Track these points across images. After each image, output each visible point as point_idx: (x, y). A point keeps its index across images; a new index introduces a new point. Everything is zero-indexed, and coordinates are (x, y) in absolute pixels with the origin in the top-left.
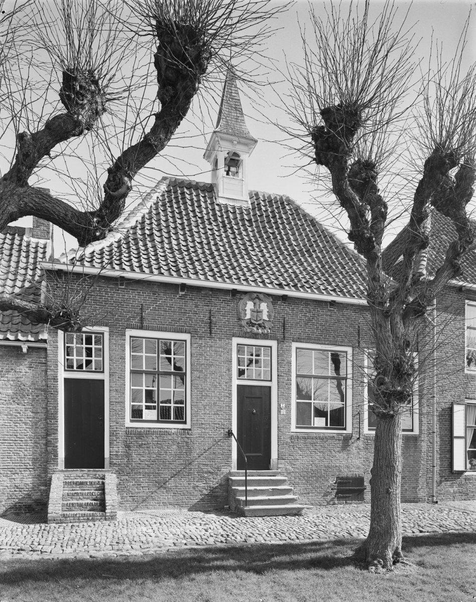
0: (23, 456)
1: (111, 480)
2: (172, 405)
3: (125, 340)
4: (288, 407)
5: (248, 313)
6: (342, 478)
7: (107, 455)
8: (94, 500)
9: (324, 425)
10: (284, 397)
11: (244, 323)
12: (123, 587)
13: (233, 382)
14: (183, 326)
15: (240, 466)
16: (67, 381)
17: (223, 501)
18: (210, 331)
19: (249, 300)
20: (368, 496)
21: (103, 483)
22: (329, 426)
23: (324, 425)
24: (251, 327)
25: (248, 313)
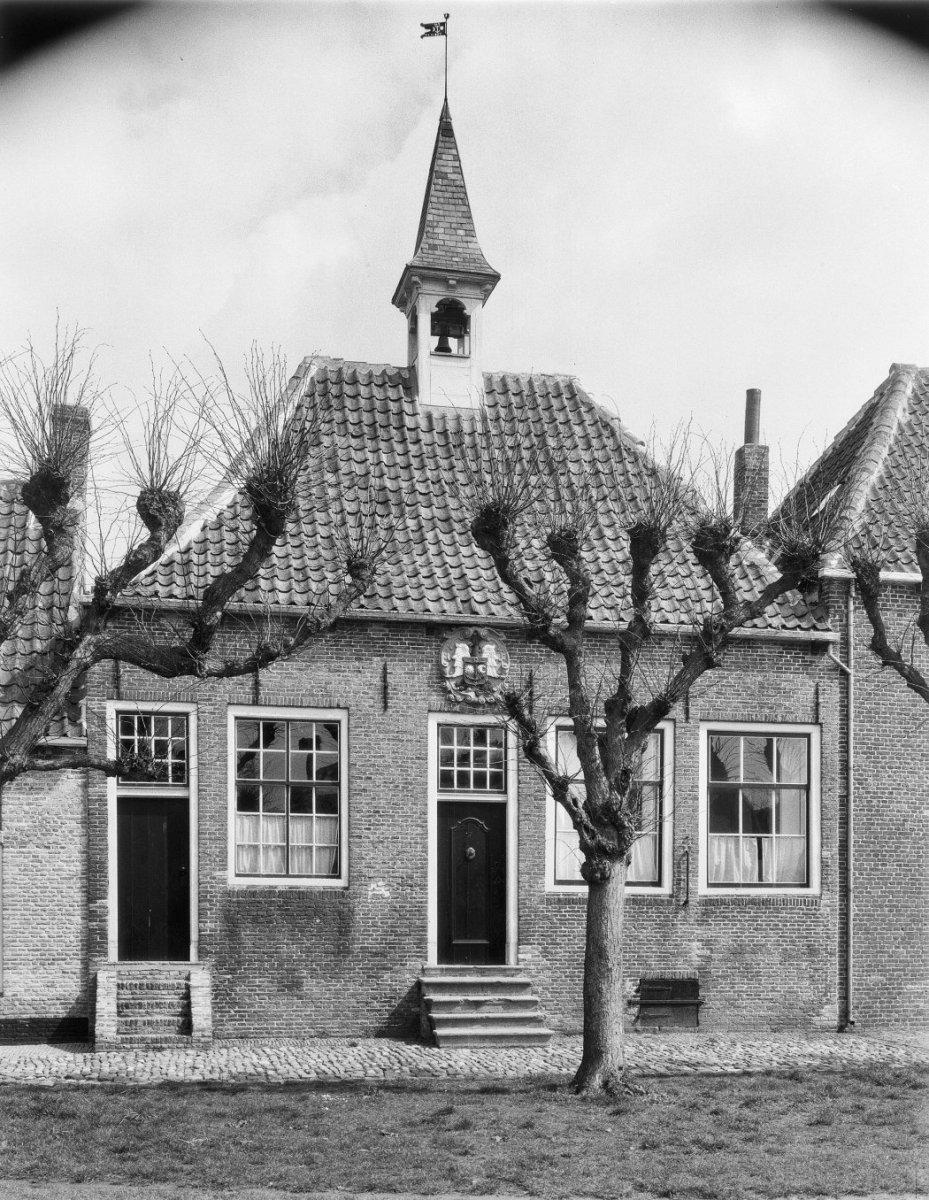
0: (47, 938)
1: (201, 979)
3: (226, 726)
6: (652, 982)
7: (194, 936)
8: (173, 1015)
12: (681, 1029)
15: (447, 953)
17: (412, 1022)
18: (386, 703)
19: (462, 641)
21: (188, 987)
24: (463, 693)
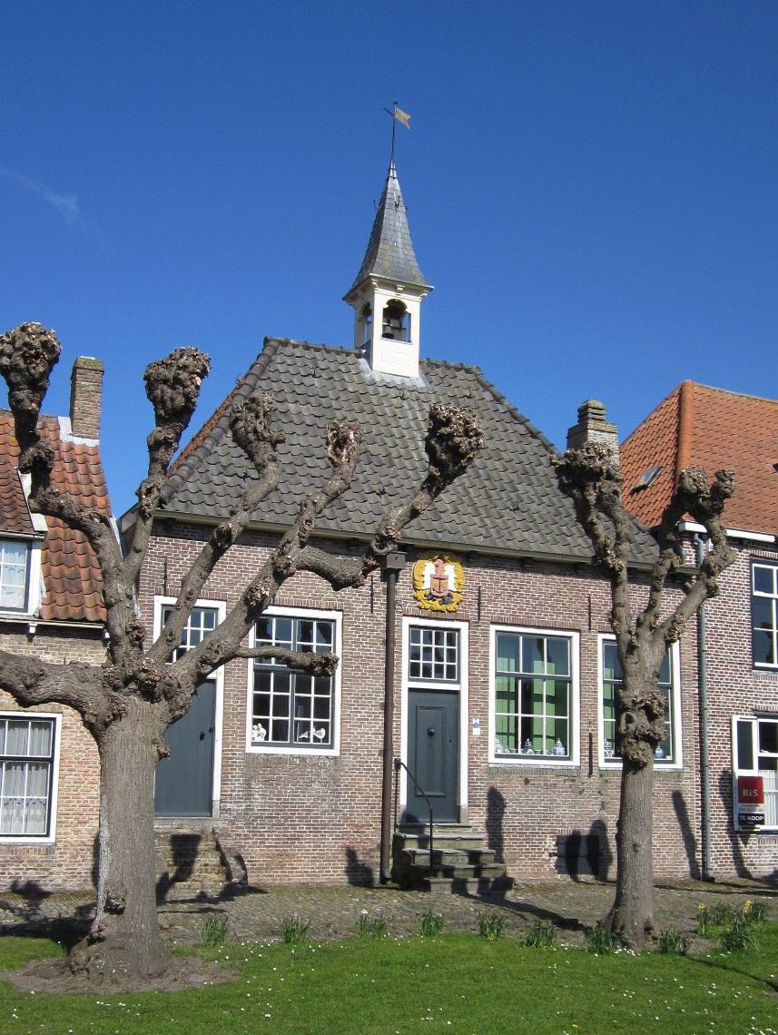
2: (312, 719)
4: (484, 723)
5: (427, 579)
7: (216, 795)
9: (262, 739)
10: (479, 710)
11: (420, 595)
13: (402, 685)
14: (331, 600)
16: (760, 758)
20: (735, 784)
22: (270, 740)
23: (262, 739)
24: (431, 602)
25: (427, 579)
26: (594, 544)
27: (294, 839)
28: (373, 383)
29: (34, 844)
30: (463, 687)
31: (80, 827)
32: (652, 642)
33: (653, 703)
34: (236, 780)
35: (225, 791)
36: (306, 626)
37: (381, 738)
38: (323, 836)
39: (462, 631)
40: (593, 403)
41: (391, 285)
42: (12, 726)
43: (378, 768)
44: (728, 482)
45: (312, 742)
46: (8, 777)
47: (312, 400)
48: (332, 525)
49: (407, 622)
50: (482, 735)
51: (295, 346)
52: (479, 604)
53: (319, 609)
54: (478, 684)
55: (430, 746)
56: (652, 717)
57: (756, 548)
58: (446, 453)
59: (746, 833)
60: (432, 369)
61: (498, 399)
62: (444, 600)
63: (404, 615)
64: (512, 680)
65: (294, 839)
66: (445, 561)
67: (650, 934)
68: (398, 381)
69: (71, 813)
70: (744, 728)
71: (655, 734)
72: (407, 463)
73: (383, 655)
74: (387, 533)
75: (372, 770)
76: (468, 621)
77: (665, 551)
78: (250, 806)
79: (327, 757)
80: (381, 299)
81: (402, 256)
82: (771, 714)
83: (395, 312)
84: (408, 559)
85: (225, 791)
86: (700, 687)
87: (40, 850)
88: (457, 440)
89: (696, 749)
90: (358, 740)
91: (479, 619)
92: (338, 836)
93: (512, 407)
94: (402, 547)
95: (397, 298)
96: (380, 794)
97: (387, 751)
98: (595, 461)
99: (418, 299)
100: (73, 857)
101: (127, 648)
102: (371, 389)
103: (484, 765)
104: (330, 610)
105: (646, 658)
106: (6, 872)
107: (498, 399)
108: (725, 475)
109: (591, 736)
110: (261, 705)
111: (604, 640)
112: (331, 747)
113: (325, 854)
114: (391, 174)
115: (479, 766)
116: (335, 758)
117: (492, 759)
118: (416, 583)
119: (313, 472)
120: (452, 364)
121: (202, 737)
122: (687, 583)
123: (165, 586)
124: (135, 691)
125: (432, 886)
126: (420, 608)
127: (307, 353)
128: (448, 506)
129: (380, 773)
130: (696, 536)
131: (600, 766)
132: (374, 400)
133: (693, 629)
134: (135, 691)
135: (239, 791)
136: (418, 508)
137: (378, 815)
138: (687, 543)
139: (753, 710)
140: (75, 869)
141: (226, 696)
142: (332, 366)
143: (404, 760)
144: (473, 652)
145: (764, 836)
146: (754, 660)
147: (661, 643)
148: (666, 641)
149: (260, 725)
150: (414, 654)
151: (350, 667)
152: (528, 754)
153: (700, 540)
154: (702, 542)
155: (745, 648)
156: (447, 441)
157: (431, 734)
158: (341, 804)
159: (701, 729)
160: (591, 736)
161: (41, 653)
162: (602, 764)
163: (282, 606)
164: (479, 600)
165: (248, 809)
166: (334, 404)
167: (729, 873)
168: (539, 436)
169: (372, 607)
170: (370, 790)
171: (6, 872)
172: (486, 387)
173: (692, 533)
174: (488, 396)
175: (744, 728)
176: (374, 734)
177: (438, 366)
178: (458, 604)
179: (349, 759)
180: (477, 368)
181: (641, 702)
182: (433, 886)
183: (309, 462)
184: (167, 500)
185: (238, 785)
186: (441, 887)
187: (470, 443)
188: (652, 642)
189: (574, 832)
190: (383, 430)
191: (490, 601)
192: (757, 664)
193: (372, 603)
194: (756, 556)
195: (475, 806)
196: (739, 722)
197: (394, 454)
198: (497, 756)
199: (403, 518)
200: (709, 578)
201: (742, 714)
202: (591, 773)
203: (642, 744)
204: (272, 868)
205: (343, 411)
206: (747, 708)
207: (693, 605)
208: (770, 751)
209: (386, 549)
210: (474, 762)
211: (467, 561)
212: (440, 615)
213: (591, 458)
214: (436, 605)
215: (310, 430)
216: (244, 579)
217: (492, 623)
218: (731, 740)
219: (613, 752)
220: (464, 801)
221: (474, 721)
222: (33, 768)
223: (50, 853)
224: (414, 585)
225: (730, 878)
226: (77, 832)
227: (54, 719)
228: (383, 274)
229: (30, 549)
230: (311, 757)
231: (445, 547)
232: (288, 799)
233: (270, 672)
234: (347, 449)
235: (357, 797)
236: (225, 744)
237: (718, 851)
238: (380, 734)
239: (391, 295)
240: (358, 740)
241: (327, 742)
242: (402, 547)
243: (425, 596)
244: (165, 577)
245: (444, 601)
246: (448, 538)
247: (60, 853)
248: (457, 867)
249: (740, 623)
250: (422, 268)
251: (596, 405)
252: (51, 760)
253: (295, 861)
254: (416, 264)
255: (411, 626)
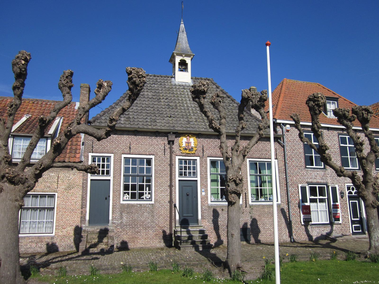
4: (206, 191)
5: (184, 143)
7: (110, 218)
11: (182, 149)
24: (185, 151)
25: (184, 143)
26: (208, 119)
27: (138, 232)
28: (175, 85)
29: (47, 236)
30: (198, 179)
31: (63, 230)
32: (238, 156)
33: (236, 179)
34: (117, 213)
35: (113, 217)
36: (142, 160)
37: (169, 197)
38: (148, 231)
39: (197, 160)
40: (252, 87)
41: (181, 55)
42: (48, 197)
43: (168, 207)
44: (265, 95)
45: (144, 199)
46: (39, 213)
47: (153, 91)
48: (150, 127)
49: (177, 158)
50: (205, 195)
51: (151, 76)
52: (203, 151)
53: (146, 155)
54: (204, 178)
55: (187, 199)
56: (237, 185)
57: (305, 127)
58: (132, 85)
59: (306, 225)
60: (196, 80)
61: (218, 87)
62: (190, 150)
63: (176, 156)
64: (216, 175)
65: (138, 232)
66: (190, 137)
67: (240, 269)
68: (184, 84)
69: (60, 225)
70: (303, 189)
71: (237, 191)
72: (182, 108)
73: (169, 169)
74: (112, 117)
75: (165, 208)
76: (199, 156)
77: (240, 122)
78: (122, 221)
79: (150, 204)
80: (178, 59)
81: (185, 46)
82: (313, 183)
83: (183, 64)
84: (176, 137)
85: (113, 217)
86: (286, 175)
87: (49, 238)
88: (134, 79)
89: (285, 197)
90: (161, 198)
91: (203, 156)
92: (154, 231)
93: (222, 89)
94: (174, 133)
95: (183, 59)
96: (169, 216)
97: (171, 201)
98: (202, 87)
99: (190, 59)
100: (60, 240)
101: (3, 165)
102: (174, 87)
103: (206, 205)
104: (150, 155)
105: (235, 162)
106: (37, 245)
107: (218, 87)
108: (263, 92)
109: (246, 193)
110: (126, 187)
111: (249, 161)
112: (151, 201)
113: (149, 237)
114: (181, 23)
115: (205, 205)
116: (152, 204)
117: (209, 203)
118: (180, 145)
119: (148, 112)
120: (203, 78)
121: (106, 199)
122: (279, 140)
123: (92, 150)
124: (6, 181)
125: (181, 248)
126: (182, 153)
127: (154, 78)
128: (194, 120)
129: (168, 209)
130: (281, 124)
131: (250, 203)
132: (175, 90)
133: (282, 155)
134: (6, 181)
135: (118, 216)
136: (124, 107)
137: (168, 223)
138: (278, 127)
139: (306, 182)
140: (61, 244)
141: (114, 185)
142: (162, 81)
143: (177, 206)
144: (201, 166)
145: (313, 226)
146: (306, 165)
147: (241, 157)
148: (243, 155)
149: (127, 194)
150: (181, 169)
151: (157, 173)
152: (223, 200)
153: (283, 126)
154: (284, 126)
155: (302, 161)
156: (131, 80)
157: (188, 195)
158: (154, 220)
159: (287, 189)
160: (246, 193)
161: (50, 173)
162: (250, 203)
163: (133, 154)
164: (203, 149)
165: (121, 223)
166: (160, 92)
167: (301, 239)
168: (230, 97)
169: (165, 153)
170: (165, 215)
171: (37, 245)
172: (214, 84)
173: (280, 124)
174: (214, 87)
175: (303, 189)
176: (166, 196)
177: (198, 79)
178: (195, 151)
179: (158, 205)
180: (212, 79)
181: (232, 179)
182: (181, 248)
183: (148, 109)
184: (93, 122)
185: (118, 214)
186: (184, 248)
187: (140, 80)
188: (238, 156)
189: (52, 243)
190: (176, 98)
191: (207, 150)
192: (307, 167)
193: (165, 152)
194: (304, 130)
195: (204, 219)
196: (301, 187)
197: (178, 105)
198: (211, 202)
199: (119, 112)
200: (260, 131)
201: (303, 184)
202: (246, 207)
203: (233, 195)
204: (130, 242)
205: (163, 93)
206: (304, 182)
207: (254, 141)
208: (314, 196)
209: (113, 124)
210: (203, 204)
211: (198, 137)
212: (189, 155)
213: (200, 86)
214: (187, 151)
215: (150, 100)
216: (120, 146)
217: (208, 157)
218: (299, 193)
219: (255, 199)
220: (200, 217)
221: (202, 190)
222: (49, 211)
223: (53, 239)
224: (179, 145)
225: (301, 241)
226: (62, 232)
227: (55, 195)
228: (178, 51)
229: (47, 140)
230: (144, 204)
231: (189, 132)
232: (136, 219)
233: (144, 176)
234: (103, 89)
235: (160, 217)
236: (113, 201)
237: (296, 232)
238: (168, 195)
239: (181, 58)
240: (161, 198)
241: (150, 199)
242: (174, 133)
243: (183, 149)
244: (93, 147)
245: (190, 150)
246: (191, 129)
247: (56, 239)
248: (196, 241)
249: (300, 153)
250: (191, 49)
251: (253, 88)
252: (54, 208)
253: (138, 240)
254: (189, 48)
255: (179, 159)
